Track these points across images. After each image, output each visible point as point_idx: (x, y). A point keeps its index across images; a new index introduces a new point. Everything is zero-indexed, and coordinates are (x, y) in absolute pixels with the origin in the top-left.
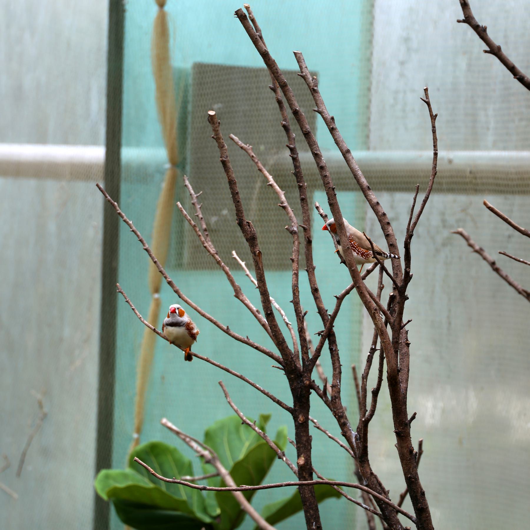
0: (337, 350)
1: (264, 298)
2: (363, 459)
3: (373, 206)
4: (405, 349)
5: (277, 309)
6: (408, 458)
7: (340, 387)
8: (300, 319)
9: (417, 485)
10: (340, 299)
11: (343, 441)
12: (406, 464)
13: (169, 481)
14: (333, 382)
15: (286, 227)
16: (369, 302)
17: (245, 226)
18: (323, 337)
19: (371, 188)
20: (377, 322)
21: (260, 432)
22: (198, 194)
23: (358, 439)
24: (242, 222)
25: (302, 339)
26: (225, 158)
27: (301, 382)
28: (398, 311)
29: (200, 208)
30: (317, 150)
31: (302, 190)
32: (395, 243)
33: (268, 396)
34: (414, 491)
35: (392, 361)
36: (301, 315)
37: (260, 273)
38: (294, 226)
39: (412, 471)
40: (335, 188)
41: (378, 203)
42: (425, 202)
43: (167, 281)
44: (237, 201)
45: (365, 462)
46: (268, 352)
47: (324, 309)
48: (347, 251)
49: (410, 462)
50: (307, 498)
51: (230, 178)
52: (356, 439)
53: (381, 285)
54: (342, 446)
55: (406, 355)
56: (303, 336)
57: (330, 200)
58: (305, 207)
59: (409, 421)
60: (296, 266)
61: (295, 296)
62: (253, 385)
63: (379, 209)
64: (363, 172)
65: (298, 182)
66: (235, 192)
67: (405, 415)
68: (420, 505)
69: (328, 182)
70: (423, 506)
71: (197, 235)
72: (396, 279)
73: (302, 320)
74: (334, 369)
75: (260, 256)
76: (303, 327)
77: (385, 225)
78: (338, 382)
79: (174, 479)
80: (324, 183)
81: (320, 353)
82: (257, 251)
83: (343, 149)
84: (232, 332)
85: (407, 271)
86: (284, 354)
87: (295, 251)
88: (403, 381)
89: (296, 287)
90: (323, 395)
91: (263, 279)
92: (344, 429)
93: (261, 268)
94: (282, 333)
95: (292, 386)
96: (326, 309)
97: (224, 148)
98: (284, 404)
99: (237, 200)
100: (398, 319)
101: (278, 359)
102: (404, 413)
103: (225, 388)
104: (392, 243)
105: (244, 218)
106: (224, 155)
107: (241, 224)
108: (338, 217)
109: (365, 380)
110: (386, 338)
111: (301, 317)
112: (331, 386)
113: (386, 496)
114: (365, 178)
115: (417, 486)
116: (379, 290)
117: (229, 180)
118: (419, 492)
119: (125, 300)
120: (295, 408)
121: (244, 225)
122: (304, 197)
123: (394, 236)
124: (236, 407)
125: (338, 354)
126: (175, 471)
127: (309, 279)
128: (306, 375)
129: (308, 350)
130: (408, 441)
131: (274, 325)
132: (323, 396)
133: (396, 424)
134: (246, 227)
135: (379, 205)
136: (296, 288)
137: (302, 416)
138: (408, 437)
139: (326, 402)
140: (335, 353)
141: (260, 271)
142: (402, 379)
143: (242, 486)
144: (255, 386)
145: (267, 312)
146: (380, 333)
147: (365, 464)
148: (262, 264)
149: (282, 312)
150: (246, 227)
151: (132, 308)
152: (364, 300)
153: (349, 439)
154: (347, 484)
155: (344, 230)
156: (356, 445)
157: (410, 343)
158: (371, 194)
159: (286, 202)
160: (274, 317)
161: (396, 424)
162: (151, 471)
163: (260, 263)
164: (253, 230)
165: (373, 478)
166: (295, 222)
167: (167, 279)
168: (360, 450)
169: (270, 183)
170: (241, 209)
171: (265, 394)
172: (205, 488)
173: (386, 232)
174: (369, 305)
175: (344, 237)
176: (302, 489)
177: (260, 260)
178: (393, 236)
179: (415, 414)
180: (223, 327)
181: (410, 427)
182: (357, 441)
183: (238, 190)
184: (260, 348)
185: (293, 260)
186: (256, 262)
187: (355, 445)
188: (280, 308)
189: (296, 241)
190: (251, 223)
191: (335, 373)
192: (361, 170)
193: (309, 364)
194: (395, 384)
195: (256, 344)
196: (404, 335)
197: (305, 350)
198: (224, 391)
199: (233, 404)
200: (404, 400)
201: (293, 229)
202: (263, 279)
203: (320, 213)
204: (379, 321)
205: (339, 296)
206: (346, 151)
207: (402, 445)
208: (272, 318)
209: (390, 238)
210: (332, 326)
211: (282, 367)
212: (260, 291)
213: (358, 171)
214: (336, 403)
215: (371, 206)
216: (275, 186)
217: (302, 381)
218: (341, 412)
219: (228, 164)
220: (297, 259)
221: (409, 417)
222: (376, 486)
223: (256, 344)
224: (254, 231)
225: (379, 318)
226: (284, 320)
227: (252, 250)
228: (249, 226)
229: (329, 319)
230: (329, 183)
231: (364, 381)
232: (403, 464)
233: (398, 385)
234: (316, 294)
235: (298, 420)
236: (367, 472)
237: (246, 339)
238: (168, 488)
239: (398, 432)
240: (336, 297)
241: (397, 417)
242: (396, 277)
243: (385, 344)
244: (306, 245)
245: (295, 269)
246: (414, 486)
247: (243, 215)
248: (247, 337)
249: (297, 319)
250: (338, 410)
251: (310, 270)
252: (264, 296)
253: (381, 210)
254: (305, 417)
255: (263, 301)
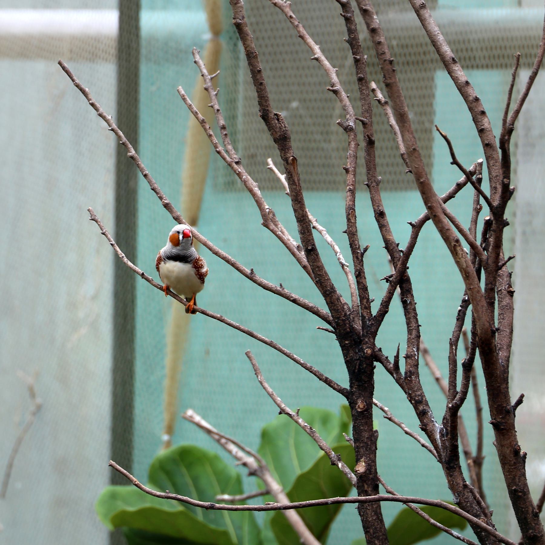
0: (412, 303)
1: (303, 227)
2: (452, 465)
3: (459, 88)
4: (506, 301)
5: (329, 244)
6: (513, 462)
7: (418, 358)
8: (357, 258)
9: (526, 502)
10: (417, 227)
11: (424, 439)
12: (509, 471)
13: (160, 495)
14: (407, 351)
15: (338, 121)
16: (447, 229)
17: (272, 121)
18: (392, 284)
19: (457, 60)
20: (460, 259)
21: (306, 426)
22: (214, 75)
23: (444, 434)
24: (268, 114)
25: (360, 287)
26: (241, 20)
27: (359, 351)
28: (493, 243)
29: (216, 95)
30: (367, 4)
31: (359, 66)
32: (492, 142)
33: (311, 372)
34: (522, 511)
35: (482, 317)
36: (359, 251)
37: (295, 189)
38: (350, 119)
39: (518, 481)
40: (393, 60)
41: (467, 83)
42: (532, 79)
43: (163, 204)
44: (259, 83)
45: (455, 468)
46: (312, 307)
47: (393, 242)
48: (412, 154)
49: (515, 468)
50: (369, 522)
51: (248, 49)
52: (442, 435)
53: (477, 205)
54: (423, 446)
55: (508, 308)
56: (362, 282)
57: (386, 79)
58: (364, 91)
59: (513, 407)
60: (352, 178)
61: (350, 224)
62: (290, 355)
63: (470, 91)
64: (444, 34)
65: (354, 54)
66: (256, 70)
67: (506, 398)
68: (531, 531)
69: (383, 51)
70: (537, 533)
71: (207, 134)
72: (495, 195)
73: (360, 258)
74: (410, 332)
75: (295, 165)
76: (362, 270)
77: (479, 115)
78: (414, 351)
79: (167, 493)
80: (377, 53)
81: (388, 308)
82: (289, 157)
83: (415, 3)
84: (259, 277)
85: (504, 182)
86: (334, 310)
87: (350, 157)
88: (503, 348)
89: (350, 210)
90: (394, 370)
91: (300, 199)
92: (423, 421)
93: (297, 182)
94: (329, 279)
95: (347, 357)
96: (397, 243)
97: (239, 5)
98: (335, 383)
99: (259, 82)
100: (493, 255)
101: (326, 316)
102: (504, 394)
103: (255, 362)
104: (487, 142)
105: (269, 109)
106: (238, 14)
107: (265, 116)
108: (398, 103)
109: (454, 347)
110: (473, 283)
111: (359, 255)
112: (404, 357)
113: (488, 519)
114: (448, 46)
115: (527, 504)
116: (475, 214)
117: (247, 52)
118: (530, 511)
119: (101, 232)
120: (352, 389)
121: (271, 118)
122: (363, 76)
123: (492, 132)
124: (270, 390)
125: (414, 309)
126: (217, 488)
127: (371, 197)
128: (366, 340)
129: (370, 303)
130: (512, 436)
131: (318, 267)
132: (393, 372)
133: (492, 411)
134: (273, 122)
135: (468, 85)
136: (351, 211)
137: (362, 402)
138: (511, 430)
139: (397, 381)
140: (410, 308)
141: (295, 187)
142: (501, 345)
143: (269, 503)
144: (292, 357)
145: (307, 248)
146: (464, 276)
147: (454, 471)
148: (299, 177)
149: (337, 248)
150: (273, 122)
151: (111, 243)
152: (440, 227)
153: (430, 435)
154: (424, 501)
155: (408, 123)
156: (441, 443)
157: (514, 291)
158: (456, 69)
159: (339, 83)
160: (317, 255)
161: (492, 411)
162: (133, 480)
163: (295, 175)
164: (283, 126)
165: (468, 492)
166: (351, 113)
167: (163, 201)
168: (447, 450)
169: (316, 56)
170: (265, 95)
171: (306, 369)
172: (213, 506)
173: (480, 126)
174: (447, 234)
175: (407, 133)
176: (363, 508)
177: (295, 170)
178: (489, 131)
179: (522, 396)
180: (245, 270)
181: (515, 416)
182: (444, 437)
183: (261, 66)
184: (300, 300)
185: (347, 171)
186: (289, 173)
187: (440, 444)
188: (333, 241)
189: (352, 142)
190: (280, 115)
191: (410, 338)
192: (442, 34)
193: (372, 324)
194: (488, 351)
195: (294, 296)
196: (505, 279)
197: (365, 303)
198: (254, 365)
199: (266, 385)
200: (503, 375)
201: (348, 124)
202: (300, 199)
203: (378, 99)
204: (462, 257)
205: (416, 222)
206: (419, 6)
207: (503, 442)
208: (315, 256)
209: (485, 135)
210: (405, 268)
211: (333, 329)
212: (296, 217)
213: (438, 34)
214: (411, 381)
215: (457, 87)
216: (323, 61)
217: (362, 350)
218: (419, 395)
219: (244, 28)
220: (353, 169)
221: (513, 401)
222: (471, 504)
223: (293, 296)
224: (285, 127)
225: (462, 254)
226: (339, 259)
227: (282, 155)
228: (278, 120)
229: (401, 257)
230: (384, 53)
231: (453, 349)
232: (505, 471)
233: (494, 352)
234: (381, 220)
235: (356, 406)
236: (458, 484)
237: (279, 288)
238: (204, 515)
239: (496, 423)
240: (410, 224)
241: (494, 401)
242: (494, 193)
243: (472, 292)
244: (366, 148)
245: (350, 184)
246: (522, 504)
247: (269, 104)
248: (281, 285)
249: (353, 257)
250: (414, 391)
251: (373, 185)
252: (302, 224)
253: (472, 93)
254: (366, 402)
255: (301, 230)
